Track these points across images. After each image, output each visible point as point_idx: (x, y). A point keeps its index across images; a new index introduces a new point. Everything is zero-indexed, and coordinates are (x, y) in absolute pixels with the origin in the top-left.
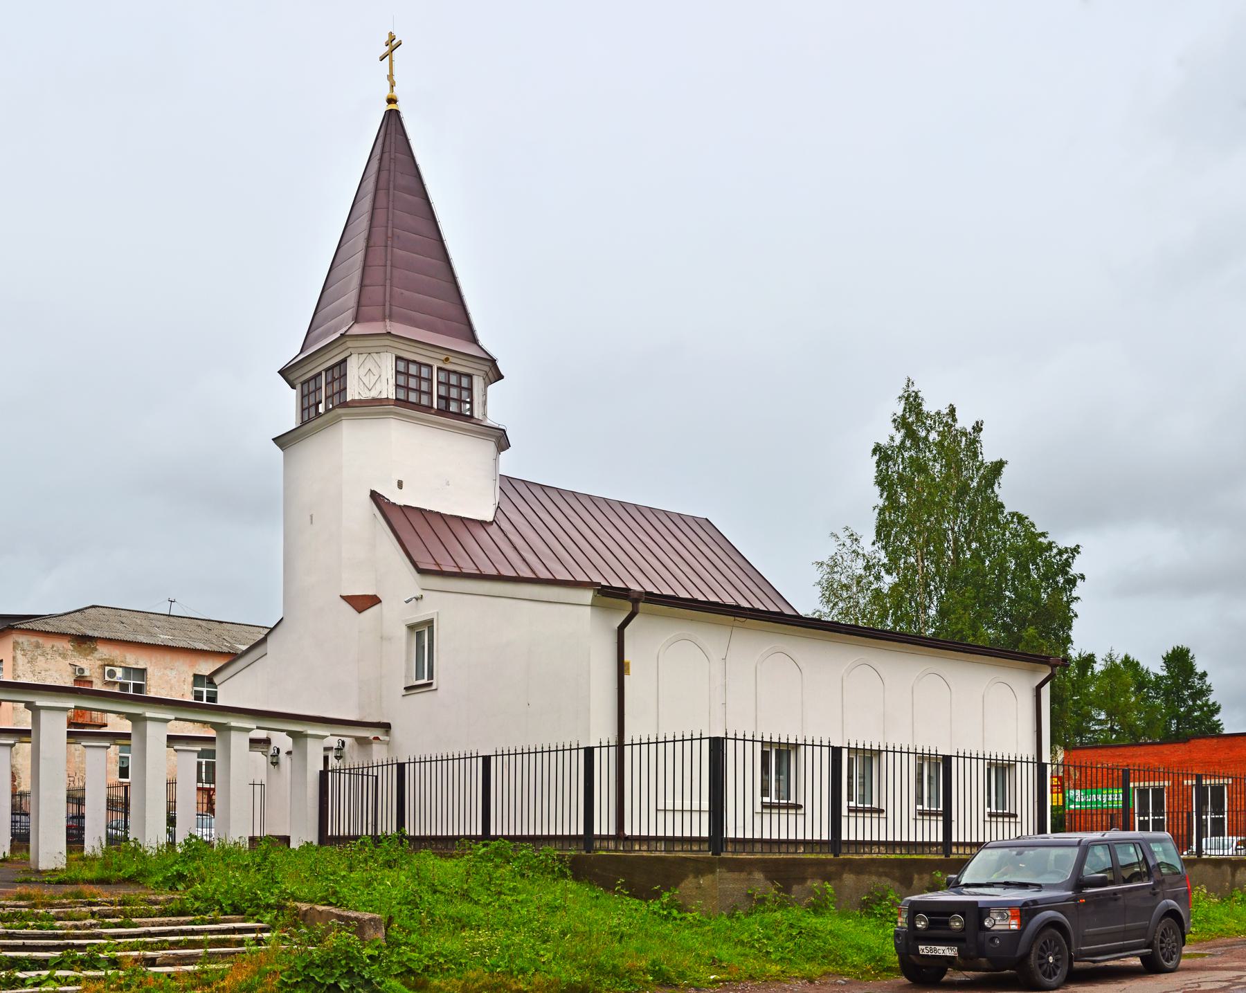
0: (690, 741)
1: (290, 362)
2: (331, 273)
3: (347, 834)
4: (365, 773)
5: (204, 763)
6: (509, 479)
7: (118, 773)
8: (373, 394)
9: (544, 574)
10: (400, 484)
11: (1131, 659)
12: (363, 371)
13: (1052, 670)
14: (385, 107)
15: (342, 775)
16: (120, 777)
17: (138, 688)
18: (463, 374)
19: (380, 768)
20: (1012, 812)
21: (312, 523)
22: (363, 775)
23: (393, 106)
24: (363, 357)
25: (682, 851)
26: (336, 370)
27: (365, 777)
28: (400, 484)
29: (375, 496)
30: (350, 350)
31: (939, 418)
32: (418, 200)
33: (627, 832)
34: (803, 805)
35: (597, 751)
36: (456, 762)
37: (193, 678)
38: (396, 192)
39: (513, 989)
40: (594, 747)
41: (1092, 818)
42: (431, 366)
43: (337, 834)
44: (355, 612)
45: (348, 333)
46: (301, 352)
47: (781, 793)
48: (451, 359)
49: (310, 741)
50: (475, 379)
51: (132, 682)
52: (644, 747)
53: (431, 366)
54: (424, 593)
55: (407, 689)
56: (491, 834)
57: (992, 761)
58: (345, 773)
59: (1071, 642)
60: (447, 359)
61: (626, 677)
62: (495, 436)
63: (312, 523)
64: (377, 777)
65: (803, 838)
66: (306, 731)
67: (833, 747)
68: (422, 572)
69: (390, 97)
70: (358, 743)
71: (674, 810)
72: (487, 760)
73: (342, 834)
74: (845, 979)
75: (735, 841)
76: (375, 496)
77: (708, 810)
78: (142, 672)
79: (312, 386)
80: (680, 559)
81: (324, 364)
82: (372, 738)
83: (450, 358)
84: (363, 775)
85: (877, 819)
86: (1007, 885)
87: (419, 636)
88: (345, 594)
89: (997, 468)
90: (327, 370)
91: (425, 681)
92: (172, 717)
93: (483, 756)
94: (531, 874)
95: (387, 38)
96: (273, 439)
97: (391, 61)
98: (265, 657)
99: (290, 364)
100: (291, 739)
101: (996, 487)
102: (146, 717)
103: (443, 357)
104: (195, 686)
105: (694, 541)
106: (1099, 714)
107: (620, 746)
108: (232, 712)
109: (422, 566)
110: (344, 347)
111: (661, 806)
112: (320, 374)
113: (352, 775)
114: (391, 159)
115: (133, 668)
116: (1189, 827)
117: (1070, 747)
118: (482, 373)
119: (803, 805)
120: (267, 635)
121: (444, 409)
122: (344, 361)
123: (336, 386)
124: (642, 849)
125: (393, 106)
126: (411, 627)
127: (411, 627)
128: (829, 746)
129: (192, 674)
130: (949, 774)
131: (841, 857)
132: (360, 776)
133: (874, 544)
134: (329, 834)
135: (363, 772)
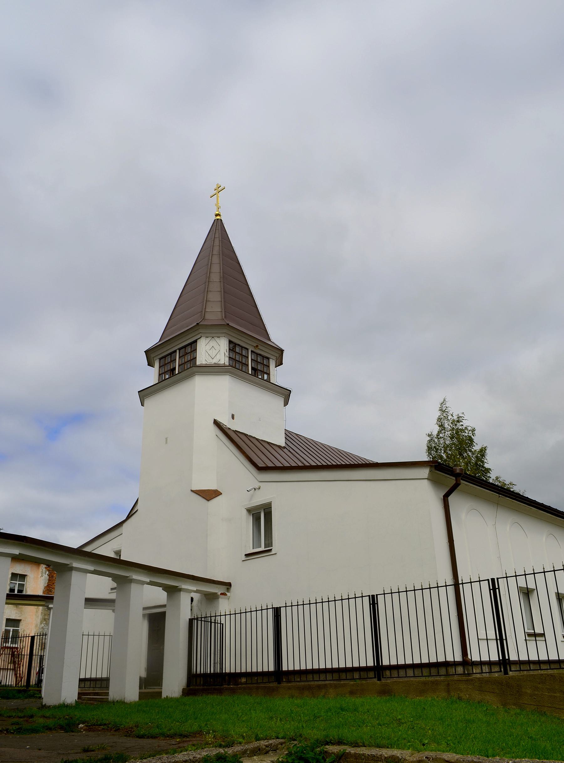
0: (398, 593)
1: (152, 346)
2: (179, 300)
3: (212, 671)
4: (213, 621)
5: (11, 630)
6: (289, 432)
7: (116, 601)
8: (215, 361)
9: (270, 465)
10: (233, 417)
11: (488, 475)
12: (208, 347)
13: (456, 480)
14: (214, 218)
15: (199, 622)
16: (53, 597)
17: (20, 591)
18: (265, 357)
19: (228, 617)
20: (538, 630)
21: (166, 443)
22: (211, 622)
23: (218, 217)
24: (208, 340)
25: (541, 669)
26: (189, 349)
27: (213, 624)
28: (233, 417)
29: (216, 423)
30: (201, 334)
31: (302, 731)
32: (264, 332)
33: (386, 662)
34: (257, 344)
35: (283, 610)
36: (295, 608)
37: (11, 575)
38: (178, 351)
39: (458, 483)
40: (280, 607)
41: (10, 653)
42: (247, 349)
43: (206, 672)
44: (144, 607)
45: (88, 549)
46: (160, 341)
47: (485, 674)
48: (259, 347)
49: (74, 574)
50: (271, 361)
51: (18, 582)
52: (326, 605)
53: (247, 349)
54: (261, 484)
55: (247, 555)
56: (283, 669)
57: (11, 668)
58: (201, 621)
59: (141, 679)
60: (257, 346)
61: (516, 489)
62: (285, 394)
63: (166, 443)
64: (223, 624)
65: (366, 666)
66: (72, 564)
67: (274, 608)
68: (261, 469)
69: (215, 214)
70: (207, 599)
71: (554, 571)
72: (277, 612)
73: (7, 684)
74: (442, 428)
75: (520, 663)
76: (216, 423)
77: (495, 638)
78: (23, 577)
79: (168, 359)
80: (310, 447)
81: (180, 345)
82: (219, 593)
83: (259, 345)
84: (211, 622)
85: (463, 576)
86: (154, 688)
87: (257, 519)
88: (194, 489)
89: (483, 452)
90: (180, 349)
91: (262, 548)
92: (148, 580)
93: (31, 636)
94: (524, 727)
95: (215, 187)
96: (222, 494)
97: (218, 197)
98: (121, 535)
99: (153, 347)
100: (166, 593)
101: (42, 618)
102: (73, 567)
103: (255, 345)
104: (11, 581)
105: (114, 539)
106: (15, 727)
107: (456, 585)
108: (445, 511)
109: (261, 465)
110: (197, 332)
111: (482, 635)
112: (175, 351)
113: (217, 624)
114: (495, 525)
115: (20, 575)
116: (482, 484)
117: (38, 610)
118: (275, 358)
119: (536, 588)
120: (265, 357)
121: (455, 674)
122: (195, 342)
123: (188, 358)
124: (393, 676)
125: (218, 217)
126: (249, 511)
127: (249, 511)
128: (272, 608)
129: (10, 573)
130: (449, 520)
131: (191, 688)
132: (209, 623)
133: (519, 490)
134: (381, 665)
135: (211, 620)
